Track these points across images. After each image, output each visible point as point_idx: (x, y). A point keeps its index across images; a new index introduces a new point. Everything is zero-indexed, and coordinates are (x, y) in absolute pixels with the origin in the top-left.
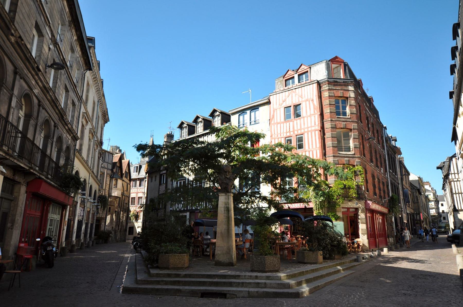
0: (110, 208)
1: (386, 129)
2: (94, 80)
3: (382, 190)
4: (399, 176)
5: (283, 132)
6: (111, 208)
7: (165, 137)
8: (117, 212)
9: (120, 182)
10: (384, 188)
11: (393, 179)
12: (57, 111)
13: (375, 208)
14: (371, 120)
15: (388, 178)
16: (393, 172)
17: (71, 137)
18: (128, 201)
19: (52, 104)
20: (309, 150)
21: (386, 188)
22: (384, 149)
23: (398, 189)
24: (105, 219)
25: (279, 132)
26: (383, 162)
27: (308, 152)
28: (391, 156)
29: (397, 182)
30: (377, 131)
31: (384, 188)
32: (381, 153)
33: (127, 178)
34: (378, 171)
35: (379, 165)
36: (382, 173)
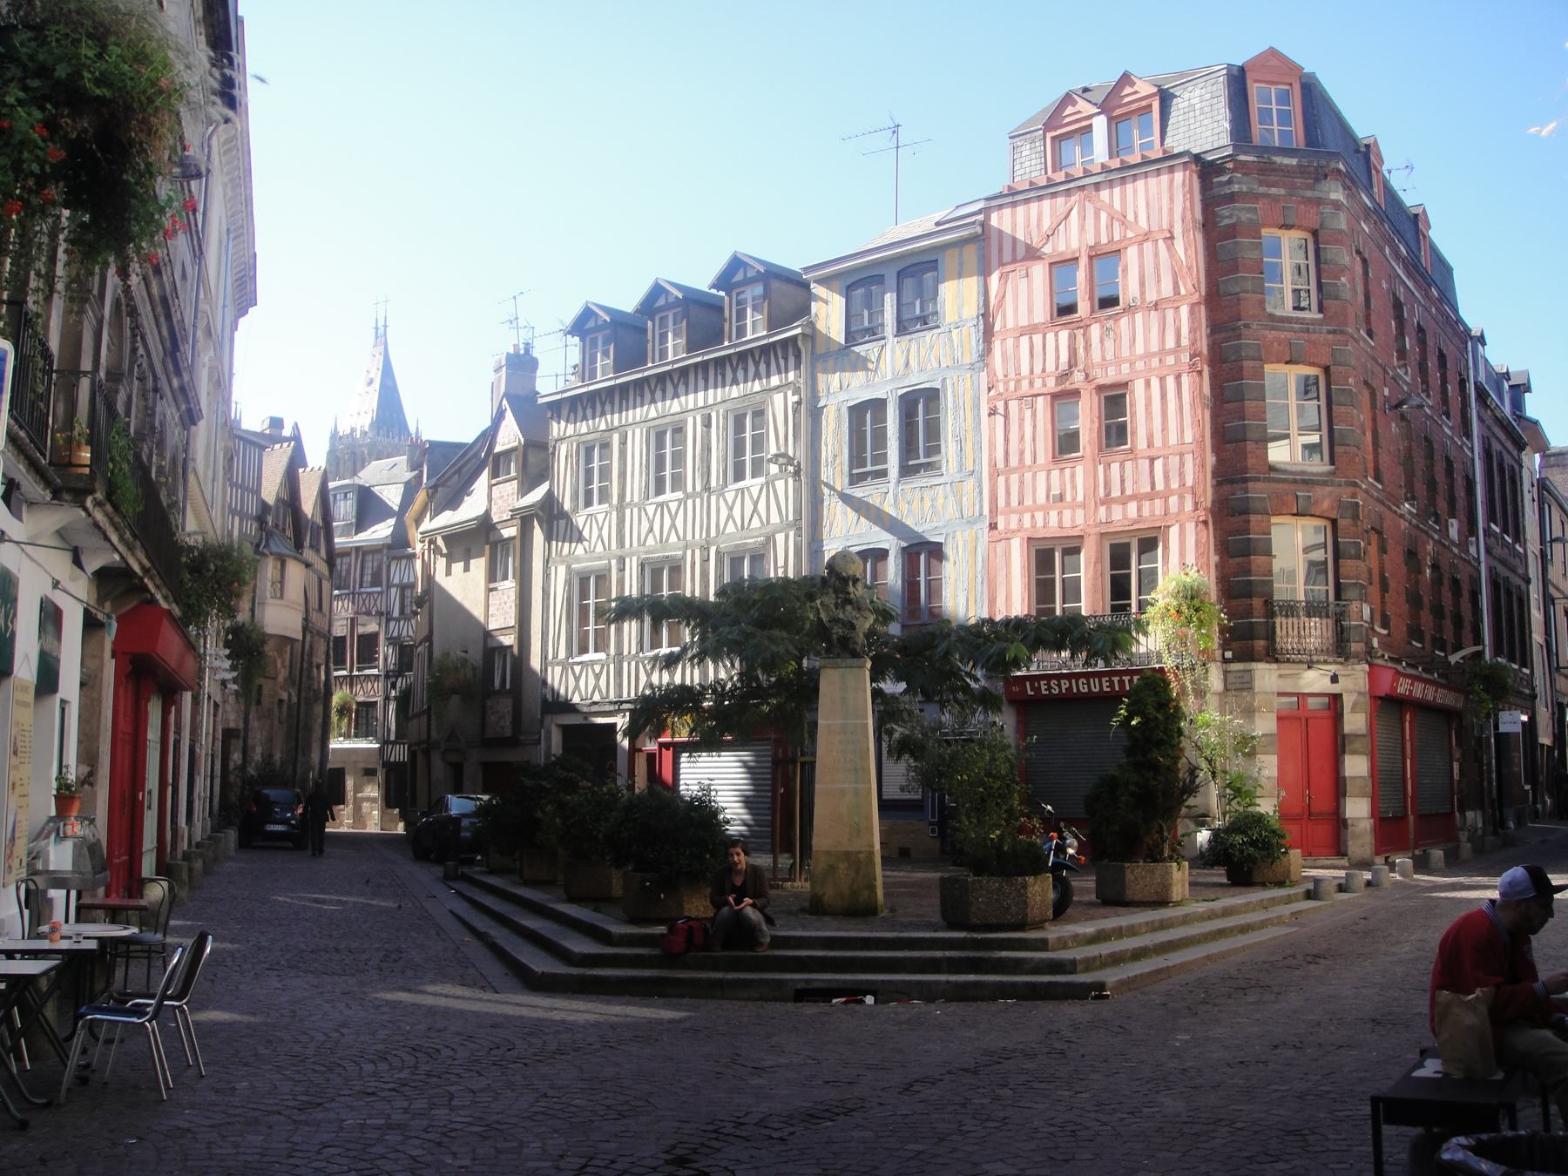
0: (260, 687)
1: (1484, 344)
2: (226, 147)
3: (1448, 614)
4: (1533, 547)
5: (1044, 370)
6: (264, 687)
7: (501, 367)
8: (285, 707)
9: (295, 572)
10: (1457, 604)
11: (1503, 562)
12: (165, 333)
13: (1411, 691)
14: (1414, 315)
15: (1478, 560)
16: (1505, 530)
17: (181, 417)
18: (323, 657)
19: (159, 309)
20: (1153, 453)
21: (1469, 605)
22: (1468, 435)
23: (1523, 602)
24: (242, 734)
25: (1025, 371)
26: (1460, 493)
27: (1147, 462)
28: (1501, 465)
29: (1520, 571)
30: (1442, 357)
31: (1457, 604)
32: (1453, 454)
33: (318, 551)
34: (1436, 537)
35: (1442, 505)
36: (1453, 543)
